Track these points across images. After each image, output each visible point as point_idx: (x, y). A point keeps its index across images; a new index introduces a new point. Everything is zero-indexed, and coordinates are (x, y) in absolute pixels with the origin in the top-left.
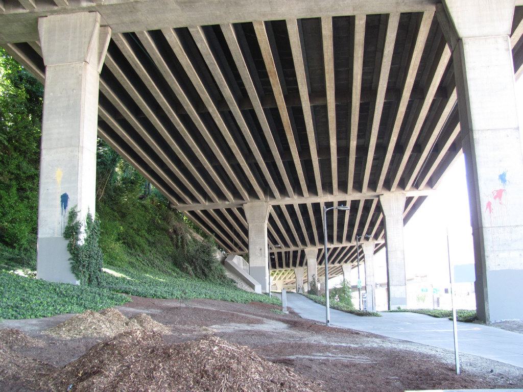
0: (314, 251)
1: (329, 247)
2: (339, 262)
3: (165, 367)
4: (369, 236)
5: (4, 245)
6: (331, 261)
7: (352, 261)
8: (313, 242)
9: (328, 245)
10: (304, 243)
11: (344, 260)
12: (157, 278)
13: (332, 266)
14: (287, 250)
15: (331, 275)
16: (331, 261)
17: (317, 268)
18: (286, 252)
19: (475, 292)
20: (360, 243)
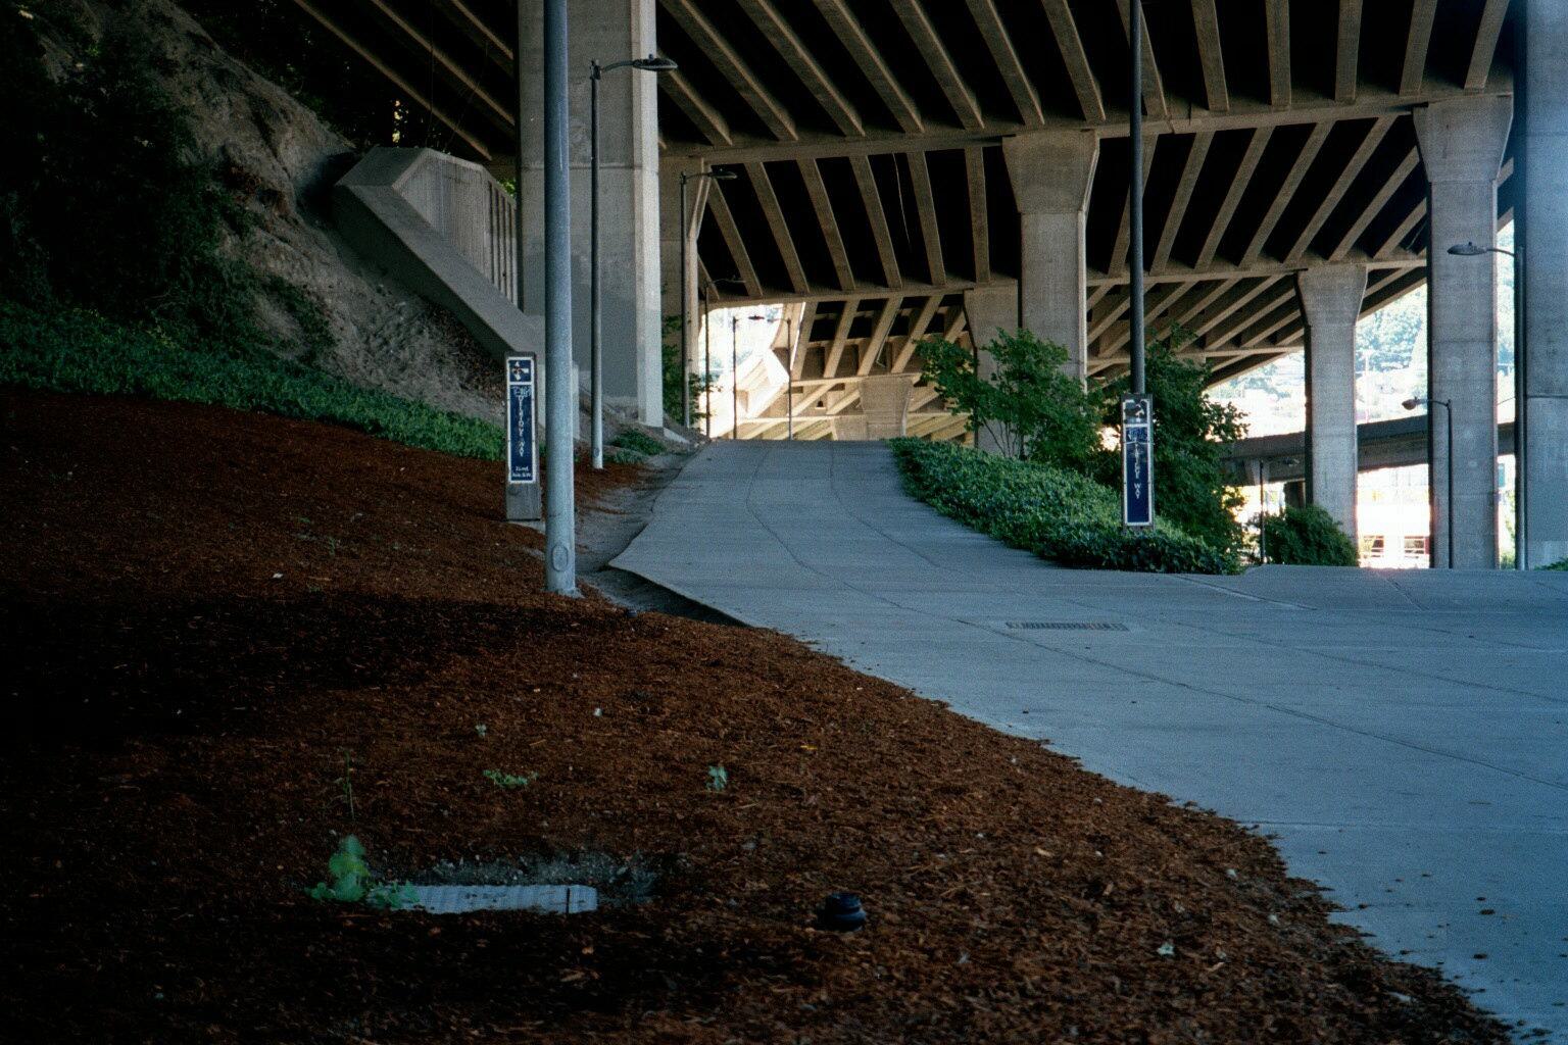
0: (1067, 154)
1: (1181, 126)
2: (1277, 248)
3: (447, 423)
4: (850, 341)
5: (358, 586)
6: (1166, 245)
7: (1369, 245)
8: (1064, 106)
9: (1162, 119)
10: (1002, 106)
11: (1308, 235)
12: (783, 941)
13: (1231, 275)
14: (889, 145)
15: (1237, 342)
16: (1166, 245)
17: (1091, 290)
18: (880, 164)
19: (1400, 570)
20: (1405, 98)
